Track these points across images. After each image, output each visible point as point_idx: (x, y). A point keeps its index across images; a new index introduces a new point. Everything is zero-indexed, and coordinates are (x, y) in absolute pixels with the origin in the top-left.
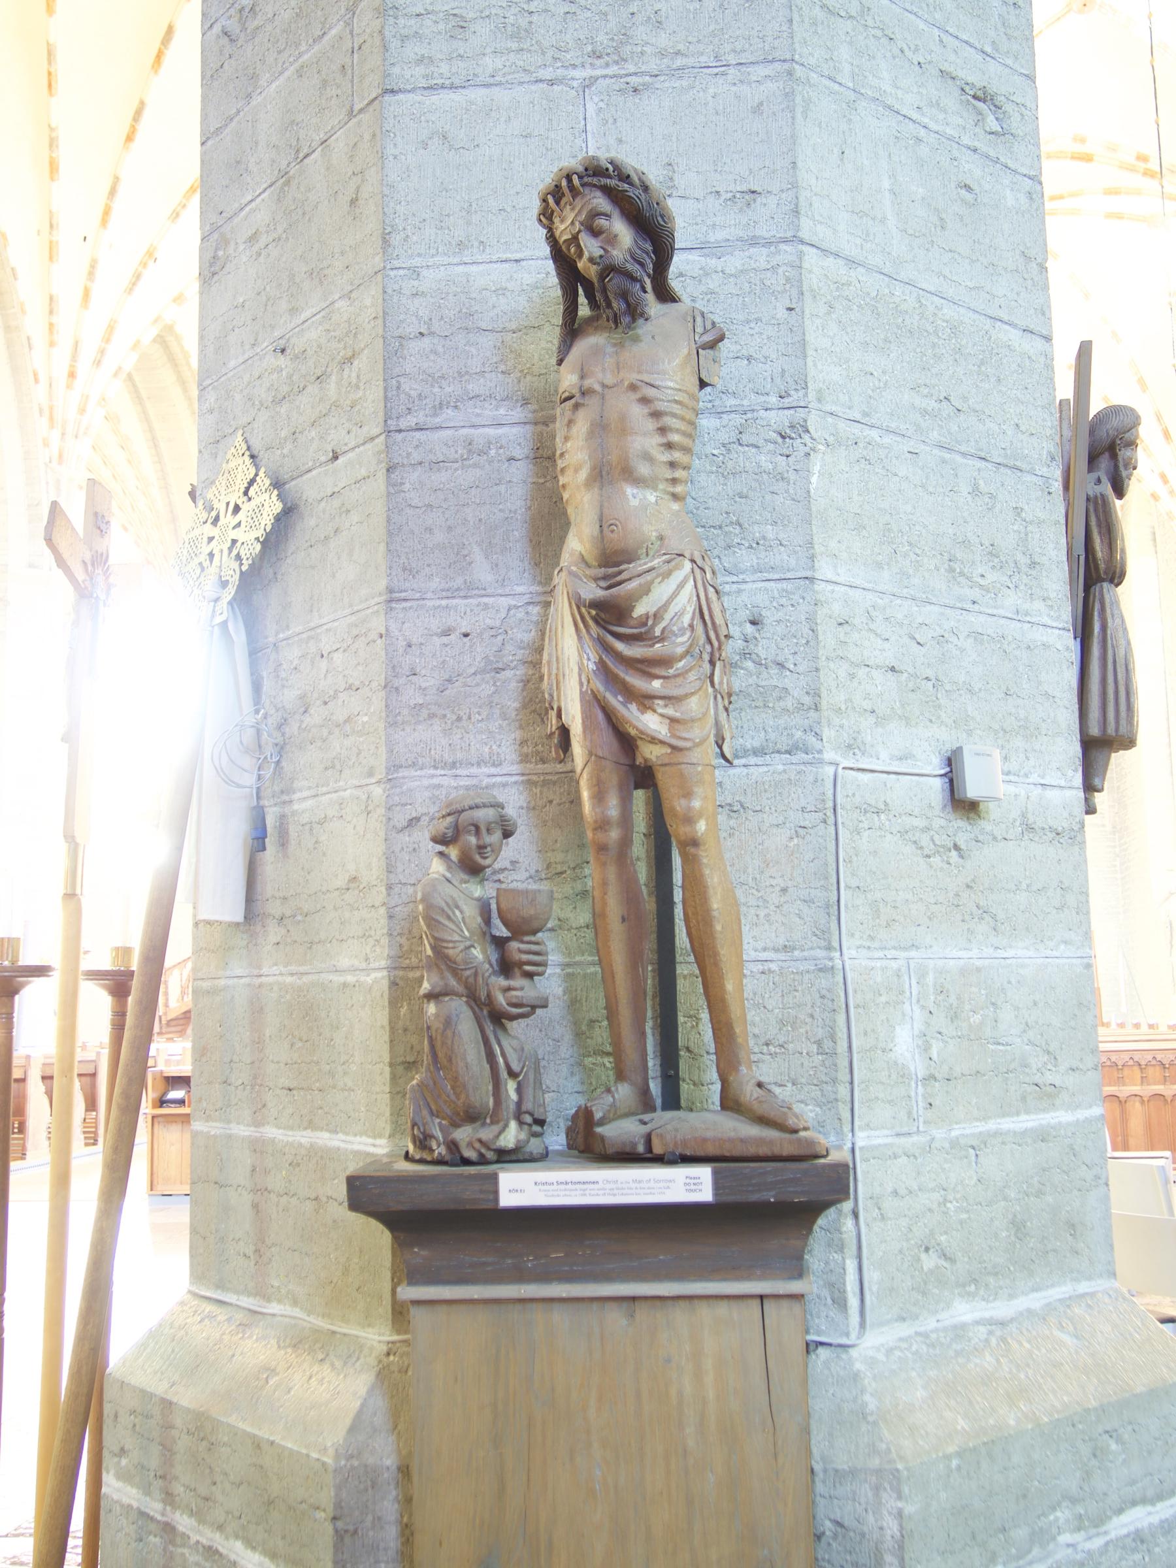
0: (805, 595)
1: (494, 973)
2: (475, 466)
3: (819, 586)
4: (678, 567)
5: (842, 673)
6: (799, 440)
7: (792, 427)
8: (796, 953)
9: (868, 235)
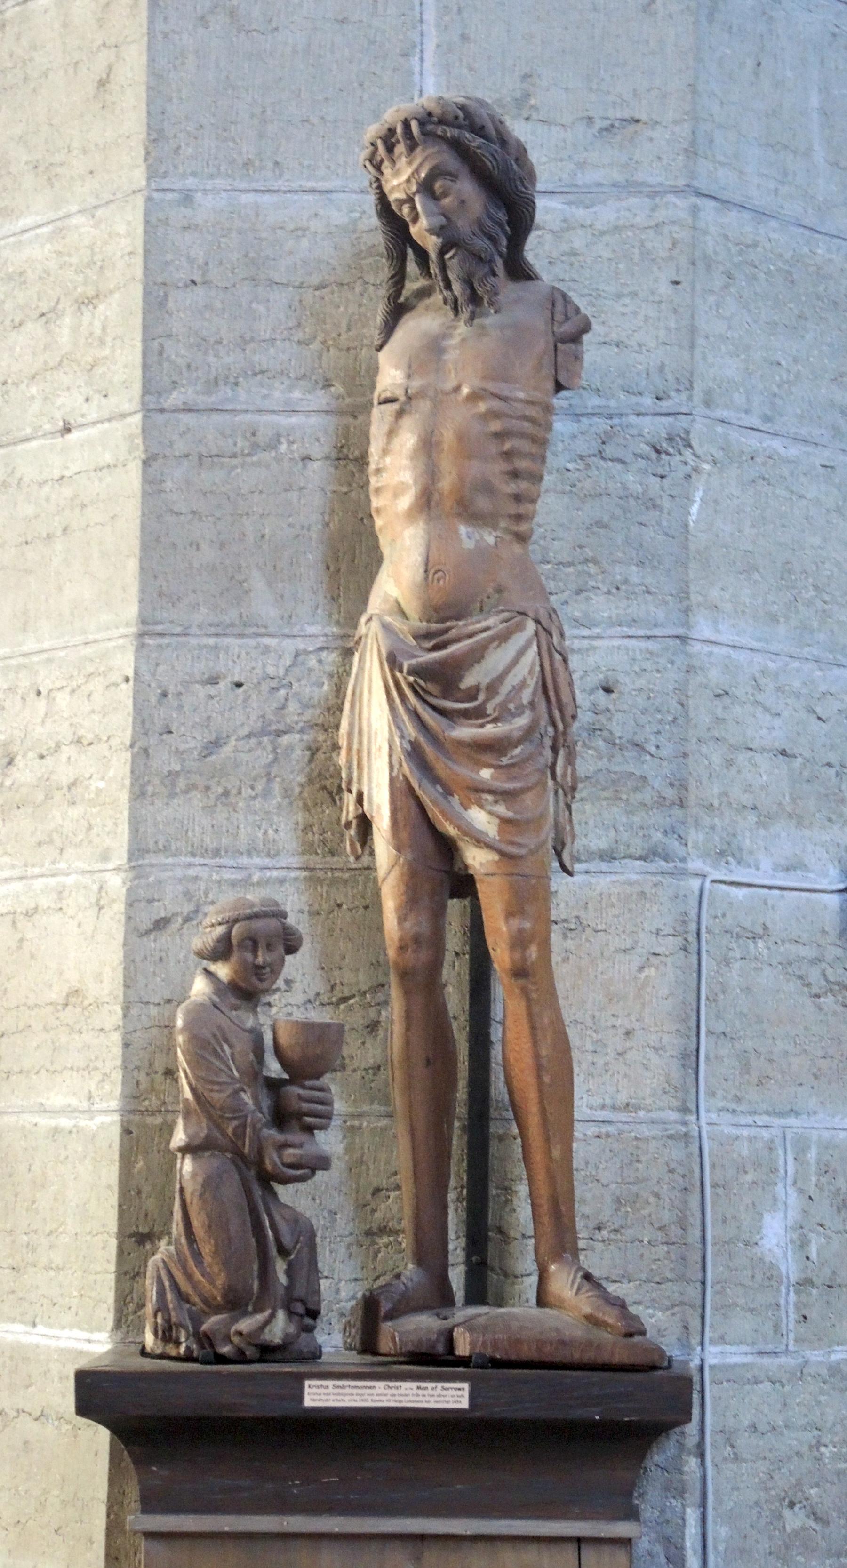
0: (674, 658)
1: (266, 1125)
2: (259, 464)
3: (696, 647)
4: (520, 627)
5: (717, 759)
6: (678, 458)
7: (670, 439)
8: (641, 1113)
9: (786, 174)
